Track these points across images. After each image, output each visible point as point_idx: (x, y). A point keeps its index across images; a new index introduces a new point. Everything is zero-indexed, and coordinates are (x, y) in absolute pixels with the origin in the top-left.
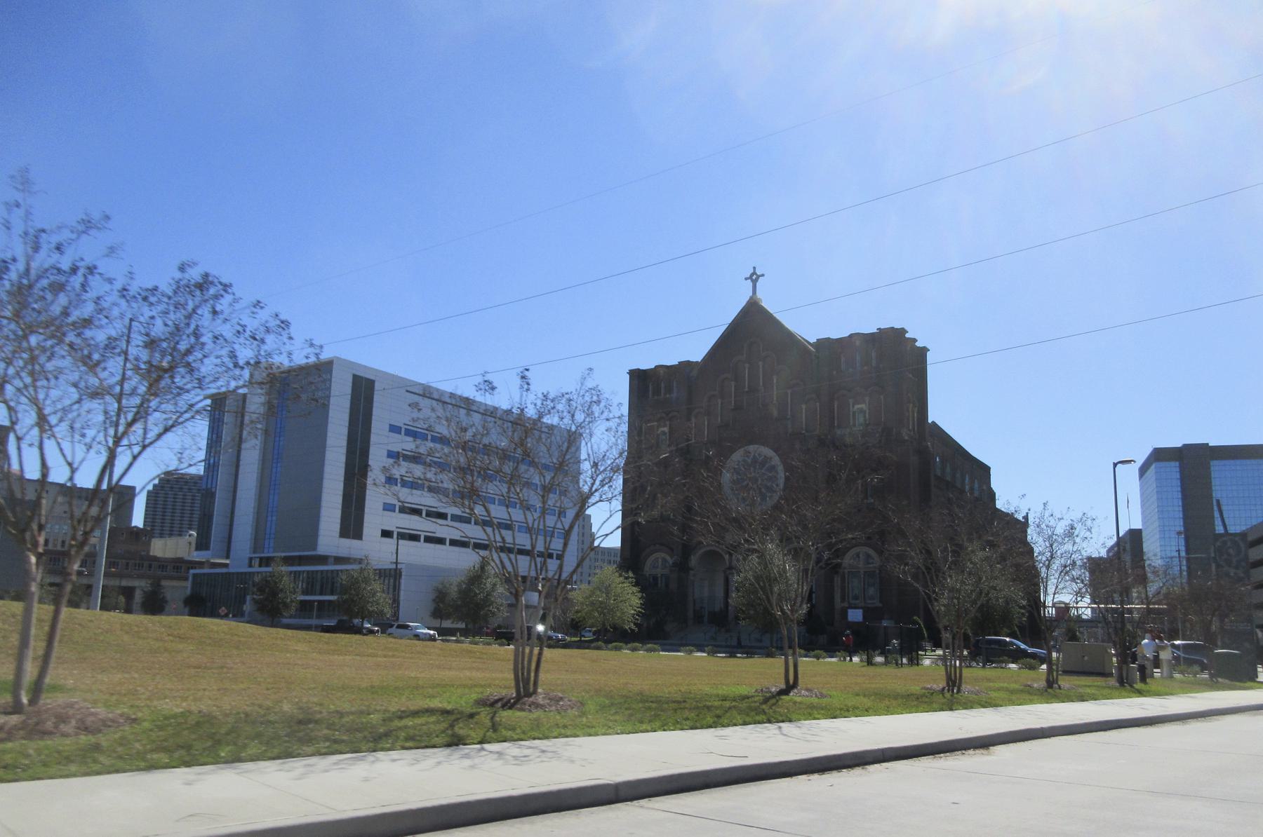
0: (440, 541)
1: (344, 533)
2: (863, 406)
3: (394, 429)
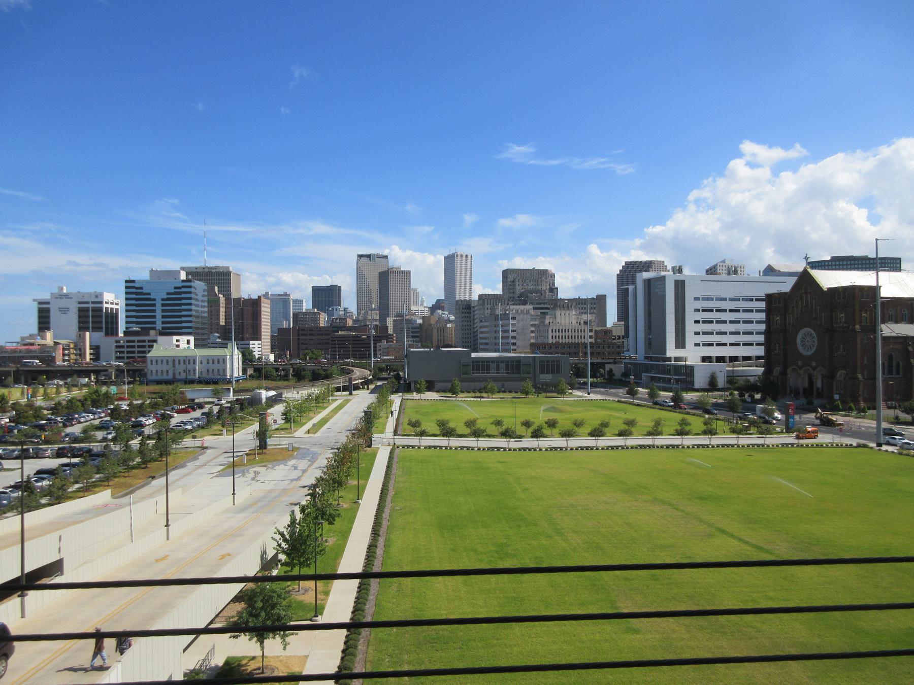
0: (725, 345)
1: (677, 347)
3: (697, 299)
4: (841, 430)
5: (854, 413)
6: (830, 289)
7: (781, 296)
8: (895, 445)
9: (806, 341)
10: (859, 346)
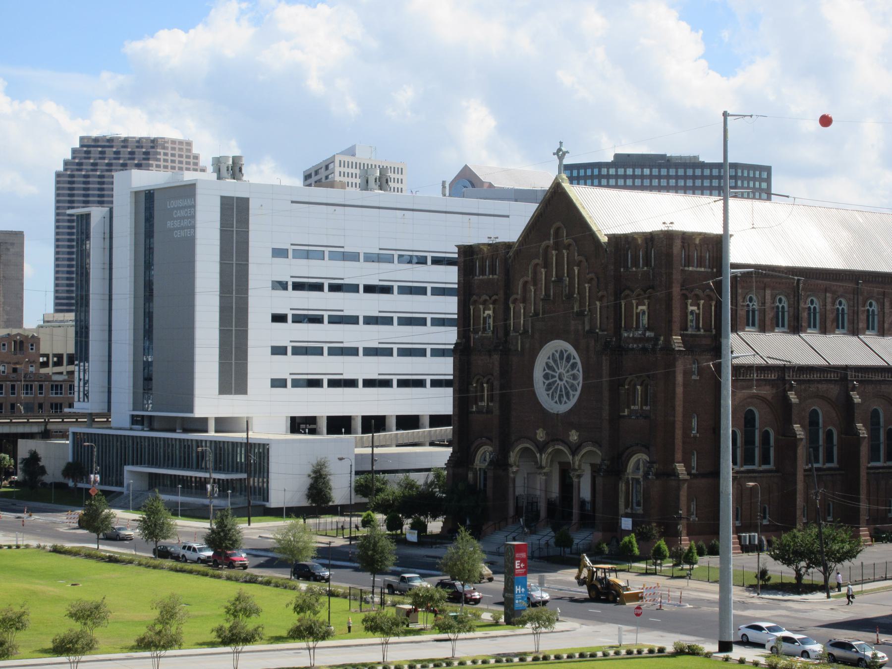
0: (351, 383)
2: (644, 308)
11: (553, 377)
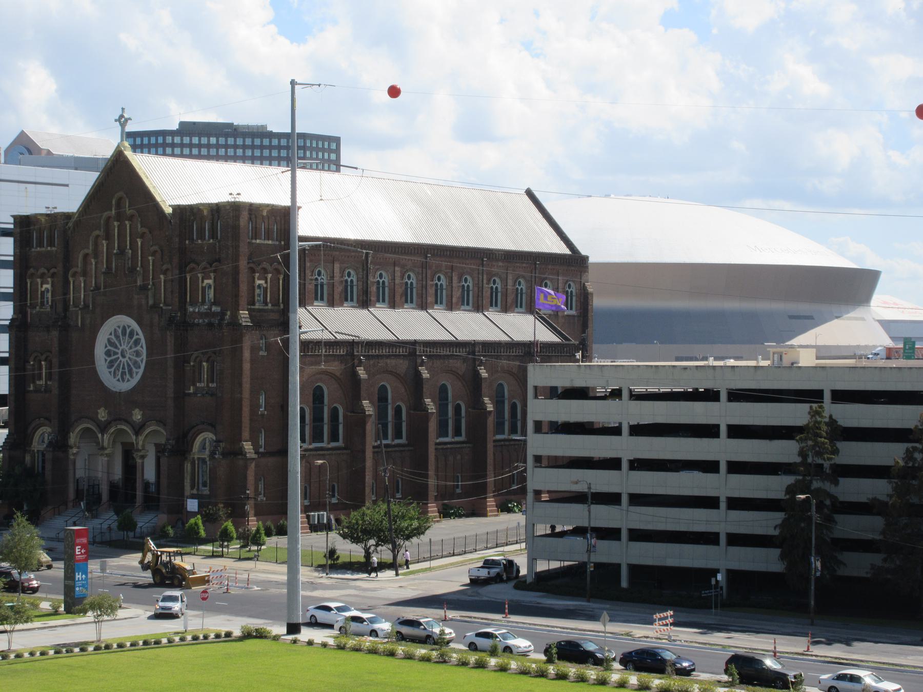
2: (210, 282)
4: (204, 596)
5: (235, 546)
6: (180, 210)
7: (57, 223)
8: (331, 626)
9: (119, 352)
10: (247, 366)
11: (115, 353)
